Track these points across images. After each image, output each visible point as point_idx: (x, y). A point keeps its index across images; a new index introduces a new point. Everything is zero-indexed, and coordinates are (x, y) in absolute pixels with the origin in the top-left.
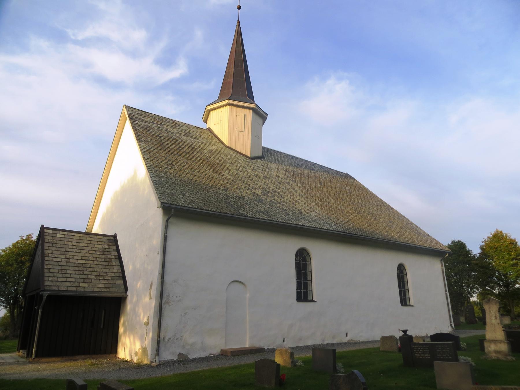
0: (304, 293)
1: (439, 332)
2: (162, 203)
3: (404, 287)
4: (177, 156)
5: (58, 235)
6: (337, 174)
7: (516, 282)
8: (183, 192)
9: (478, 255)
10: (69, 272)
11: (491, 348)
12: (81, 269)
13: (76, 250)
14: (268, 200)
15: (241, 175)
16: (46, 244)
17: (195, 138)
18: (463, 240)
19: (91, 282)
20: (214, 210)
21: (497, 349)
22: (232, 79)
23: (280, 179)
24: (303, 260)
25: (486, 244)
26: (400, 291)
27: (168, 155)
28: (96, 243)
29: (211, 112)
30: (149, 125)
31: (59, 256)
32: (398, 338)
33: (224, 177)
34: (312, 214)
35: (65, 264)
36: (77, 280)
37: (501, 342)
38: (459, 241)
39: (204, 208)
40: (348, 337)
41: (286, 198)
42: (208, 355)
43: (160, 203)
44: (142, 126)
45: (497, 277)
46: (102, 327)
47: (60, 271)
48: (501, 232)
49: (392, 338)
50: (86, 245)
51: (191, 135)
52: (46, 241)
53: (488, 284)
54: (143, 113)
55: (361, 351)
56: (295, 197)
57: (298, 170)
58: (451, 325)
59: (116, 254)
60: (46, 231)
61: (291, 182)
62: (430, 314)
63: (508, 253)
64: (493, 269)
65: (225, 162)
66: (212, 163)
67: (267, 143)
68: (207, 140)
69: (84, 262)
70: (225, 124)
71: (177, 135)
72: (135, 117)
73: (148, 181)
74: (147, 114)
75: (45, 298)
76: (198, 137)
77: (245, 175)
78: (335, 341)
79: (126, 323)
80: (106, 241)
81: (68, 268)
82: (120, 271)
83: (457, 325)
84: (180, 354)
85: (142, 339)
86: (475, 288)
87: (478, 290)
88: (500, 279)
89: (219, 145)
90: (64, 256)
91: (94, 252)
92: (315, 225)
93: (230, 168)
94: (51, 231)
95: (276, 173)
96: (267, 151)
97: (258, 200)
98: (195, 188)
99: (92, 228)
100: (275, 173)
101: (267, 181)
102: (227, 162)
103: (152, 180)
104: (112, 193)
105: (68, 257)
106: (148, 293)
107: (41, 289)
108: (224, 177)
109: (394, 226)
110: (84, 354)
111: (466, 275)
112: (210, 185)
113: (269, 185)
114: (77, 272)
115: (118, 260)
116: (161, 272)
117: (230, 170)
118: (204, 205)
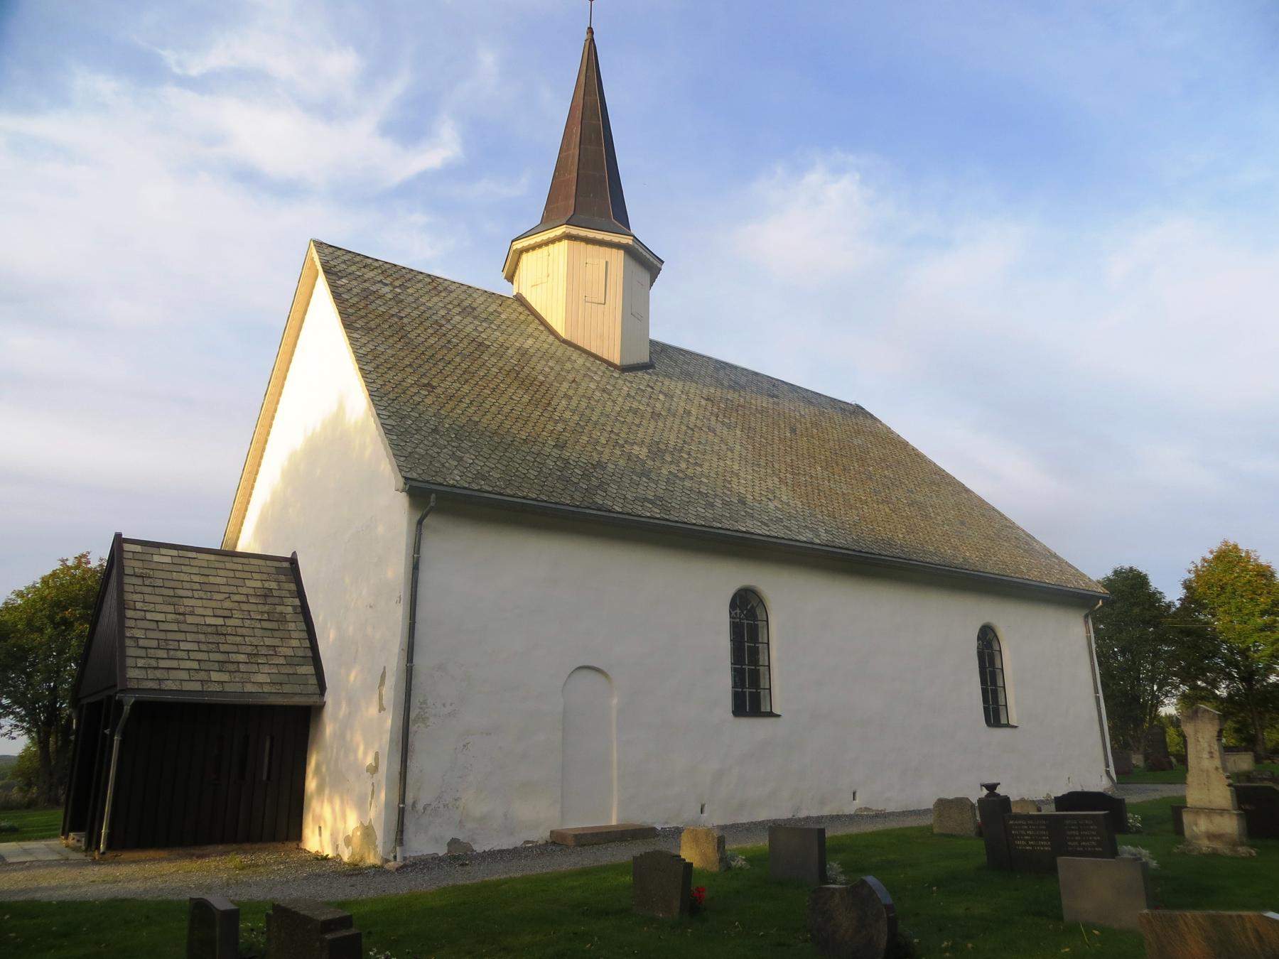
0: (750, 697)
1: (1079, 789)
2: (406, 478)
3: (994, 682)
4: (441, 365)
5: (156, 558)
9: (1178, 604)
10: (183, 646)
13: (201, 594)
14: (664, 471)
15: (598, 411)
16: (127, 580)
17: (485, 320)
18: (1142, 569)
20: (534, 496)
21: (1213, 829)
23: (693, 419)
24: (747, 616)
25: (1198, 576)
26: (985, 692)
29: (525, 256)
30: (374, 288)
31: (158, 608)
33: (556, 416)
34: (771, 505)
35: (174, 627)
37: (1222, 811)
39: (508, 491)
41: (706, 465)
43: (402, 481)
44: (355, 291)
45: (1223, 657)
46: (265, 777)
47: (163, 644)
48: (1236, 547)
49: (961, 803)
50: (223, 581)
51: (476, 313)
53: (1201, 673)
55: (888, 833)
57: (736, 396)
58: (1108, 773)
59: (297, 602)
60: (127, 547)
61: (719, 427)
62: (1057, 746)
63: (1252, 599)
64: (1215, 638)
65: (560, 378)
67: (658, 333)
68: (515, 326)
69: (220, 621)
70: (559, 285)
71: (443, 312)
74: (369, 261)
75: (127, 708)
76: (491, 318)
77: (608, 409)
78: (826, 811)
79: (324, 769)
80: (274, 571)
81: (180, 636)
83: (1124, 772)
84: (454, 842)
85: (361, 806)
86: (1168, 684)
87: (1177, 688)
88: (1231, 663)
90: (171, 609)
91: (243, 598)
92: (776, 531)
93: (571, 393)
94: (138, 548)
95: (682, 404)
96: (660, 350)
99: (238, 538)
100: (680, 404)
102: (565, 379)
104: (287, 453)
105: (182, 610)
108: (556, 416)
110: (222, 841)
113: (666, 434)
114: (203, 647)
115: (301, 618)
116: (405, 647)
117: (571, 398)
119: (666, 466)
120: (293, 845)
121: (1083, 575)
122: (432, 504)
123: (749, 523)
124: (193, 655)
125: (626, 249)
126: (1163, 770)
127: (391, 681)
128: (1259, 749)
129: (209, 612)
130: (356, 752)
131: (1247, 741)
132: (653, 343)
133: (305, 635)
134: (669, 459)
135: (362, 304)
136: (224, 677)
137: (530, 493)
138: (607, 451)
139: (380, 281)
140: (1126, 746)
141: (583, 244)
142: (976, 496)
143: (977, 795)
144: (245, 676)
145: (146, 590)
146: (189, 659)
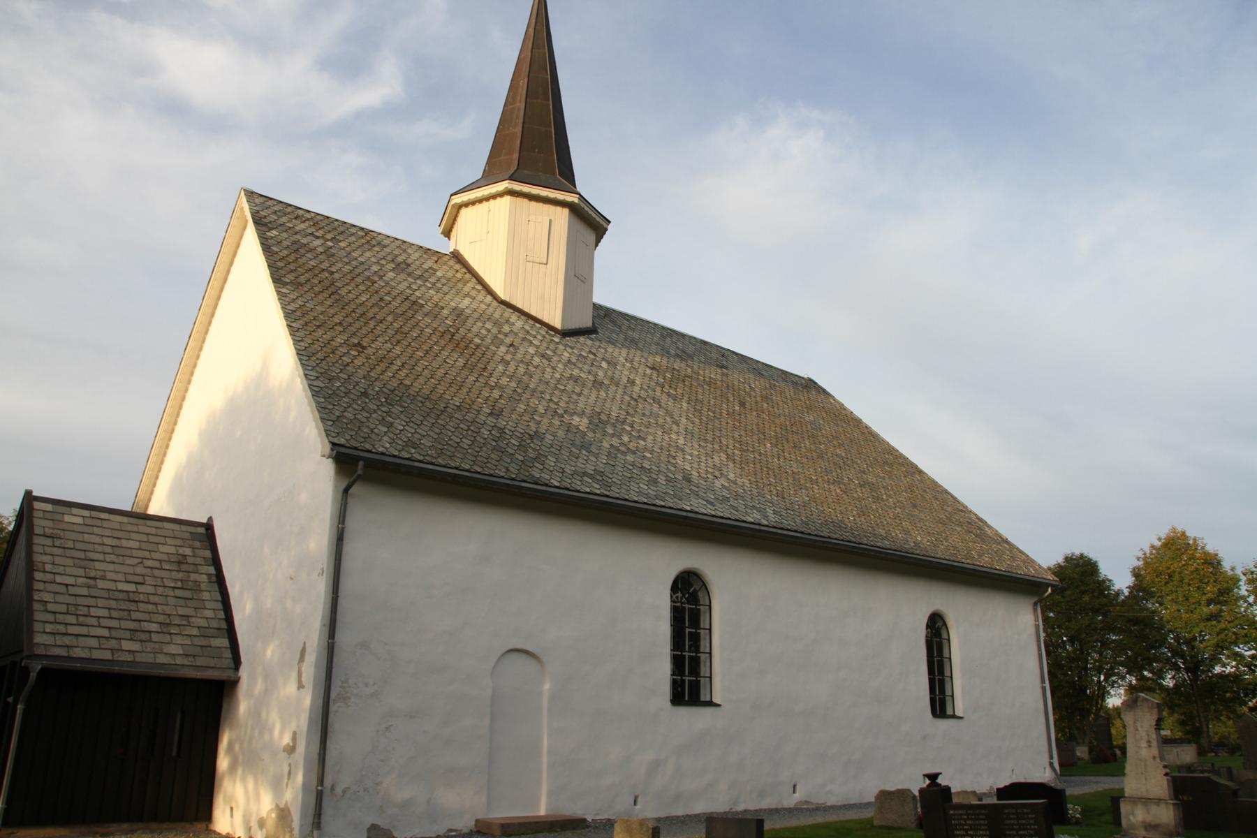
0: (688, 686)
1: (1022, 780)
2: (333, 444)
3: (941, 672)
4: (372, 323)
5: (67, 518)
6: (785, 380)
7: (1214, 660)
8: (388, 419)
9: (1126, 592)
10: (94, 612)
11: (1134, 816)
12: (124, 605)
13: (113, 558)
14: (606, 444)
15: (536, 377)
16: (36, 540)
17: (420, 277)
18: (1092, 555)
19: (150, 641)
20: (467, 467)
21: (1149, 819)
22: (520, 128)
23: (637, 389)
24: (689, 596)
25: (1146, 563)
26: (931, 682)
27: (350, 320)
28: (162, 540)
29: (464, 211)
30: (304, 241)
31: (69, 571)
32: (917, 794)
33: (493, 381)
34: (718, 483)
35: (85, 591)
36: (114, 633)
37: (1159, 801)
38: (1082, 556)
39: (440, 461)
40: (797, 795)
41: (650, 438)
42: (442, 832)
43: (328, 446)
44: (285, 243)
45: (1170, 648)
46: (174, 753)
47: (72, 609)
48: (1183, 534)
49: (903, 794)
50: (136, 545)
51: (410, 270)
52: (38, 530)
53: (1147, 663)
54: (289, 210)
55: (826, 826)
56: (674, 436)
57: (683, 365)
58: (1051, 764)
59: (212, 570)
60: (37, 505)
61: (664, 398)
62: (1002, 736)
63: (1198, 588)
64: (1162, 627)
65: (497, 342)
66: (463, 345)
67: (604, 295)
68: (451, 284)
69: (132, 587)
71: (375, 268)
72: (269, 219)
73: (299, 386)
74: (301, 212)
75: (33, 675)
76: (426, 275)
77: (548, 376)
78: (766, 804)
79: (237, 748)
80: (187, 536)
81: (91, 602)
82: (222, 615)
83: (1068, 764)
85: (277, 786)
86: (1114, 675)
87: (1123, 678)
88: (1177, 653)
89: (480, 297)
90: (81, 572)
91: (156, 564)
92: (723, 511)
93: (508, 357)
94: (49, 507)
95: (626, 373)
96: (604, 314)
97: (578, 442)
98: (413, 409)
99: (149, 500)
100: (624, 374)
101: (602, 393)
102: (502, 342)
103: (310, 385)
104: (212, 413)
105: (92, 574)
106: (294, 675)
107: (25, 653)
108: (493, 381)
109: (922, 516)
110: (129, 819)
111: (1097, 641)
112: (457, 401)
113: (608, 405)
114: (114, 614)
115: (216, 587)
116: (327, 622)
117: (508, 363)
118: (441, 453)
119: (608, 438)
120: (203, 825)
121: (1033, 561)
122: (360, 472)
123: (694, 501)
124: (104, 622)
125: (570, 206)
126: (1106, 762)
127: (311, 658)
128: (1204, 742)
129: (121, 577)
130: (271, 730)
131: (1193, 733)
132: (595, 305)
133: (220, 606)
134: (611, 431)
135: (292, 258)
136: (135, 646)
137: (463, 463)
138: (545, 421)
139: (312, 234)
140: (1072, 738)
141: (526, 201)
142: (929, 478)
143: (916, 785)
144: (157, 646)
145: (56, 551)
146: (99, 626)
